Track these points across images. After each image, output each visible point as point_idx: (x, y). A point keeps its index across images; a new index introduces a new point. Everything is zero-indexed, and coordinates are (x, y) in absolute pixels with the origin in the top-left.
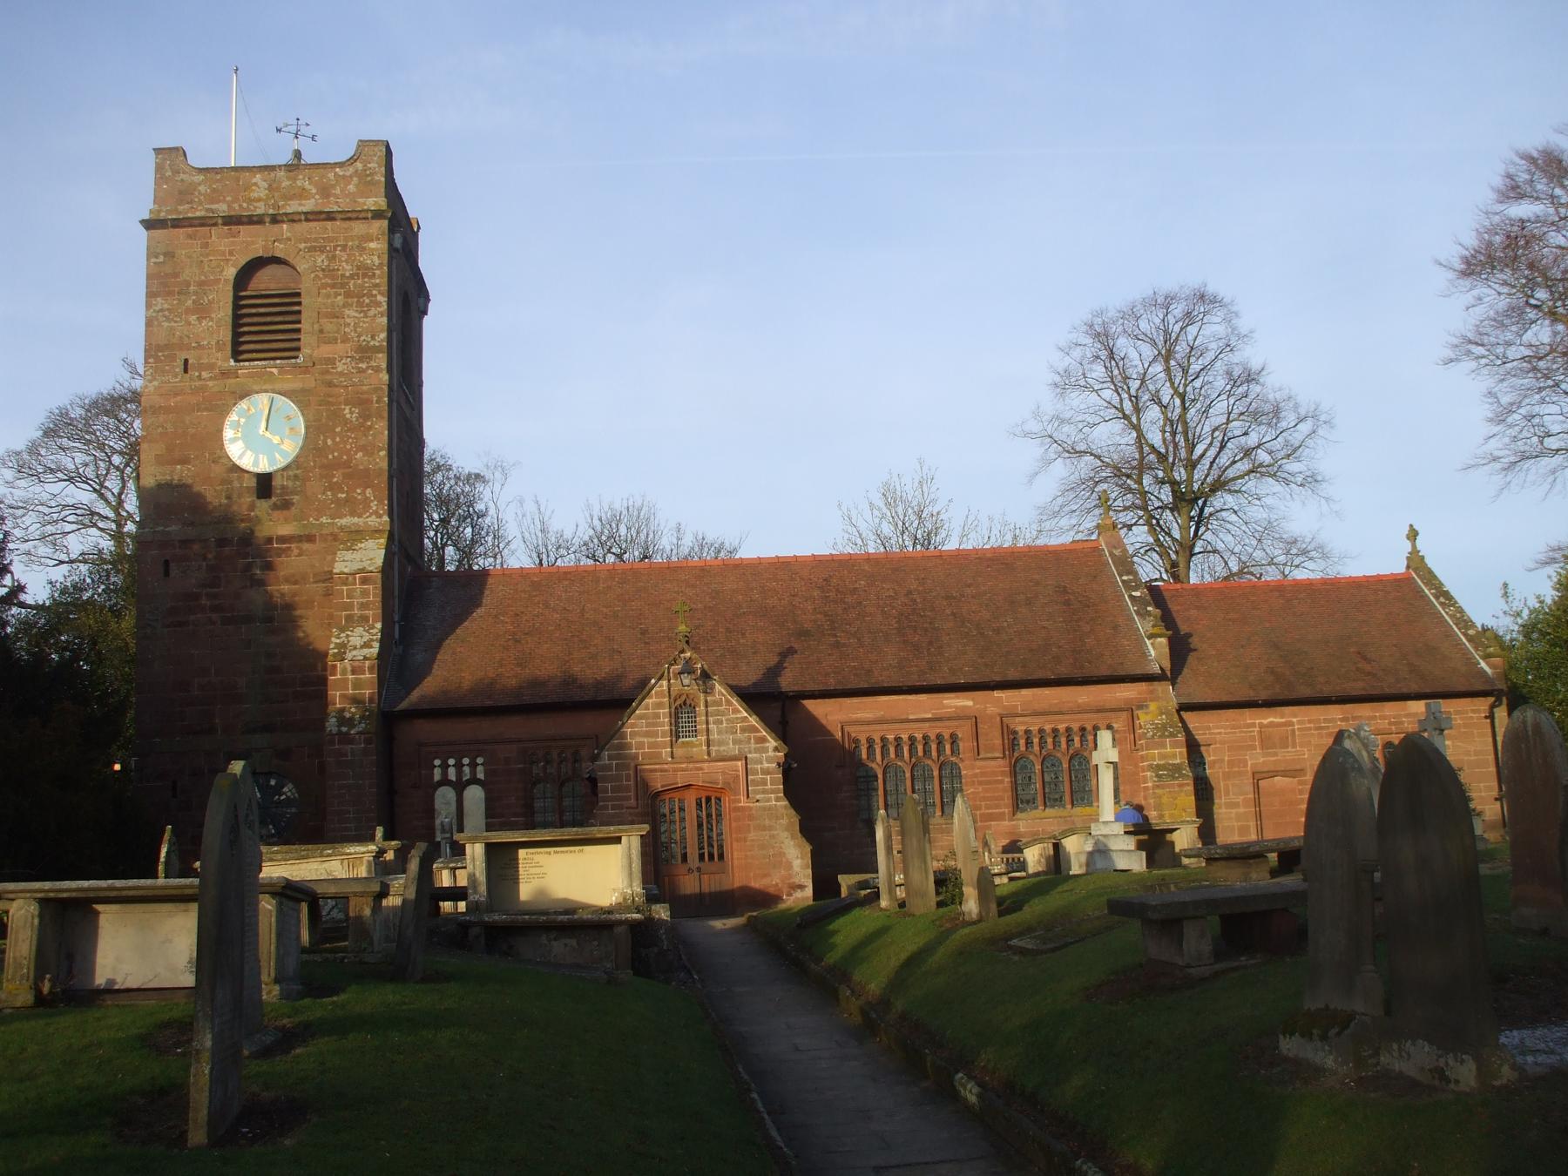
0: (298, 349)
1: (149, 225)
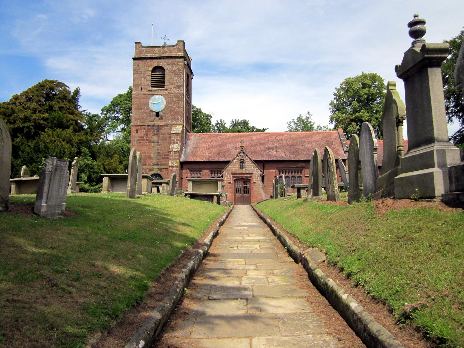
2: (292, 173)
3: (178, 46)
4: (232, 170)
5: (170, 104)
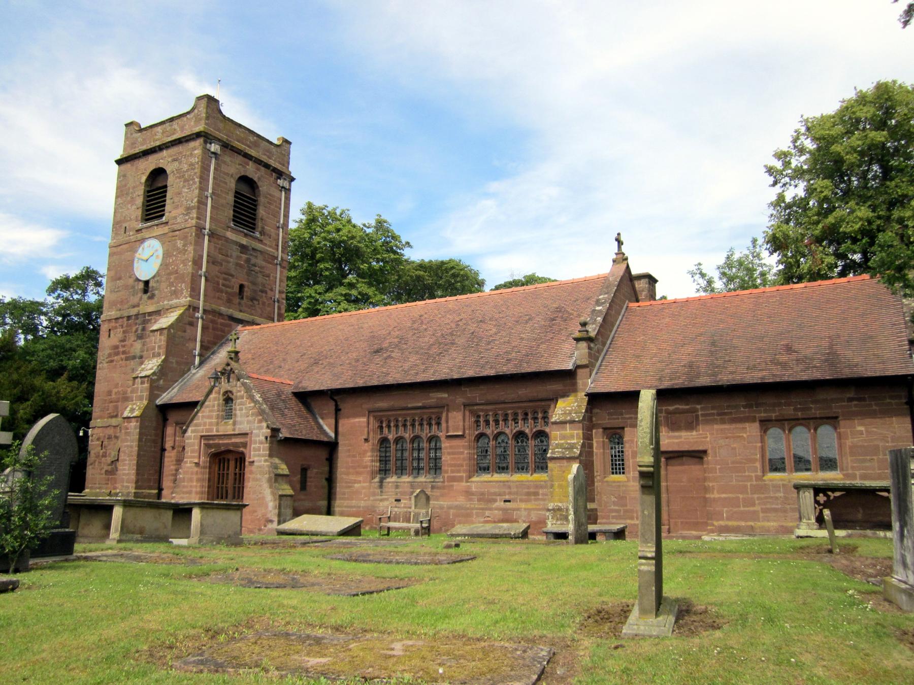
0: (163, 215)
1: (119, 162)
2: (515, 420)
3: (196, 111)
4: (205, 424)
5: (170, 256)
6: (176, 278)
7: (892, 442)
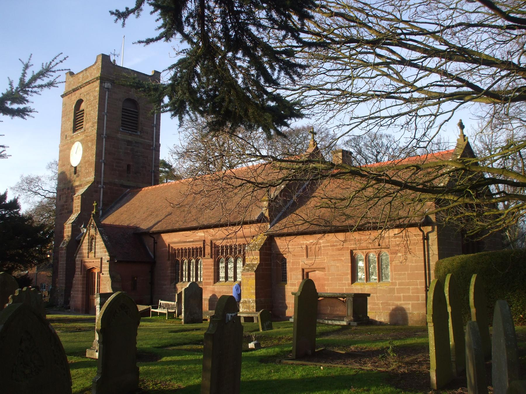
6: (89, 165)
7: (416, 262)
